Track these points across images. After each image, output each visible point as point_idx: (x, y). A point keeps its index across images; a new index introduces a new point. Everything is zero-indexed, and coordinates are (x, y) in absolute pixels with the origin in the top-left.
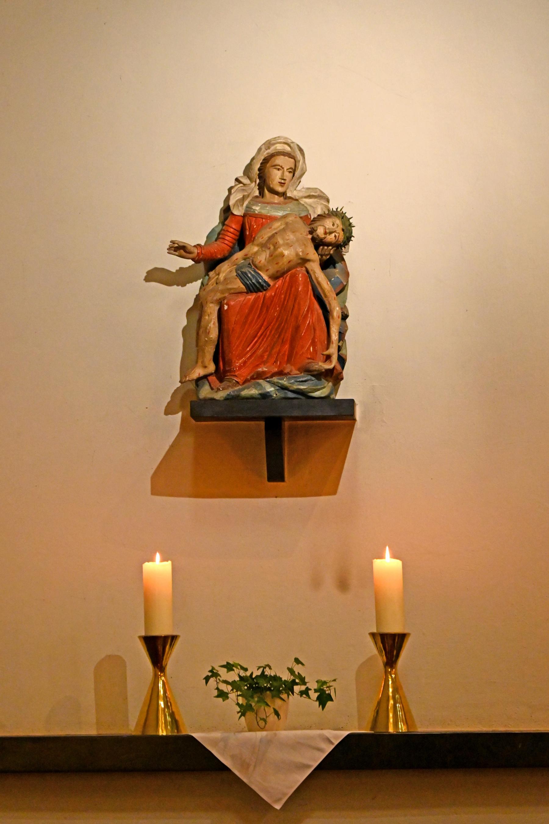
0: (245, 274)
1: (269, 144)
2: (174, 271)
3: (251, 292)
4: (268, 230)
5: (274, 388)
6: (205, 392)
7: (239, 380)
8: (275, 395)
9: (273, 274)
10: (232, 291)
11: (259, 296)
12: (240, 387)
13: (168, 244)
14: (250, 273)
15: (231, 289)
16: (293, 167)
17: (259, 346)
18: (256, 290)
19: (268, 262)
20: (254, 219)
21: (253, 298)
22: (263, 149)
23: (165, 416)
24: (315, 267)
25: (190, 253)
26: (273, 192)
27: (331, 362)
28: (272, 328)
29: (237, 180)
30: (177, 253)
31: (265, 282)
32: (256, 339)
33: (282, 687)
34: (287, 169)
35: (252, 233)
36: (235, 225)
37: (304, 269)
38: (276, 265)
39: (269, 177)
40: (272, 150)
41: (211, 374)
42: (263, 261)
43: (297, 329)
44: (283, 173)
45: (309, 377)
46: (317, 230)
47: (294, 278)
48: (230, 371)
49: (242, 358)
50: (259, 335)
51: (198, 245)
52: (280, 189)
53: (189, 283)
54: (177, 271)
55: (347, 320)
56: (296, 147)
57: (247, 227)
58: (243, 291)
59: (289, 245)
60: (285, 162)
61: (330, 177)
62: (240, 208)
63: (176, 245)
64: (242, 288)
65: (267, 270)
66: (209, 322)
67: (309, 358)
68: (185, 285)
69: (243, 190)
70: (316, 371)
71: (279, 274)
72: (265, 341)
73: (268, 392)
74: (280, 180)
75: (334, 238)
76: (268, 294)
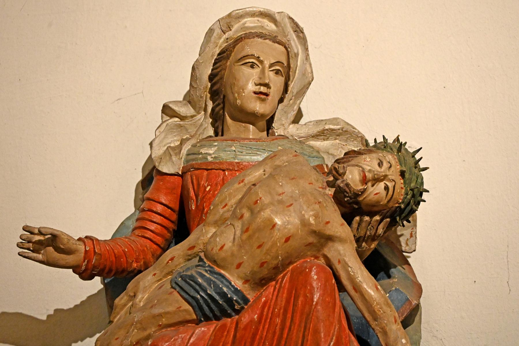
0: (189, 279)
1: (227, 22)
2: (44, 318)
3: (207, 319)
4: (236, 186)
9: (253, 273)
10: (164, 321)
11: (224, 326)
13: (17, 234)
14: (202, 276)
15: (160, 315)
18: (218, 313)
19: (240, 247)
20: (205, 173)
22: (218, 31)
24: (347, 256)
25: (68, 252)
26: (248, 117)
30: (40, 257)
31: (236, 291)
34: (271, 65)
36: (166, 194)
37: (322, 261)
38: (258, 251)
39: (232, 85)
40: (236, 31)
42: (229, 245)
44: (263, 71)
47: (300, 280)
51: (86, 237)
54: (49, 316)
56: (287, 20)
57: (192, 193)
58: (188, 317)
59: (285, 205)
61: (245, 215)
65: (239, 266)
69: (180, 126)
71: (265, 272)
74: (257, 89)
75: (384, 193)
76: (245, 318)
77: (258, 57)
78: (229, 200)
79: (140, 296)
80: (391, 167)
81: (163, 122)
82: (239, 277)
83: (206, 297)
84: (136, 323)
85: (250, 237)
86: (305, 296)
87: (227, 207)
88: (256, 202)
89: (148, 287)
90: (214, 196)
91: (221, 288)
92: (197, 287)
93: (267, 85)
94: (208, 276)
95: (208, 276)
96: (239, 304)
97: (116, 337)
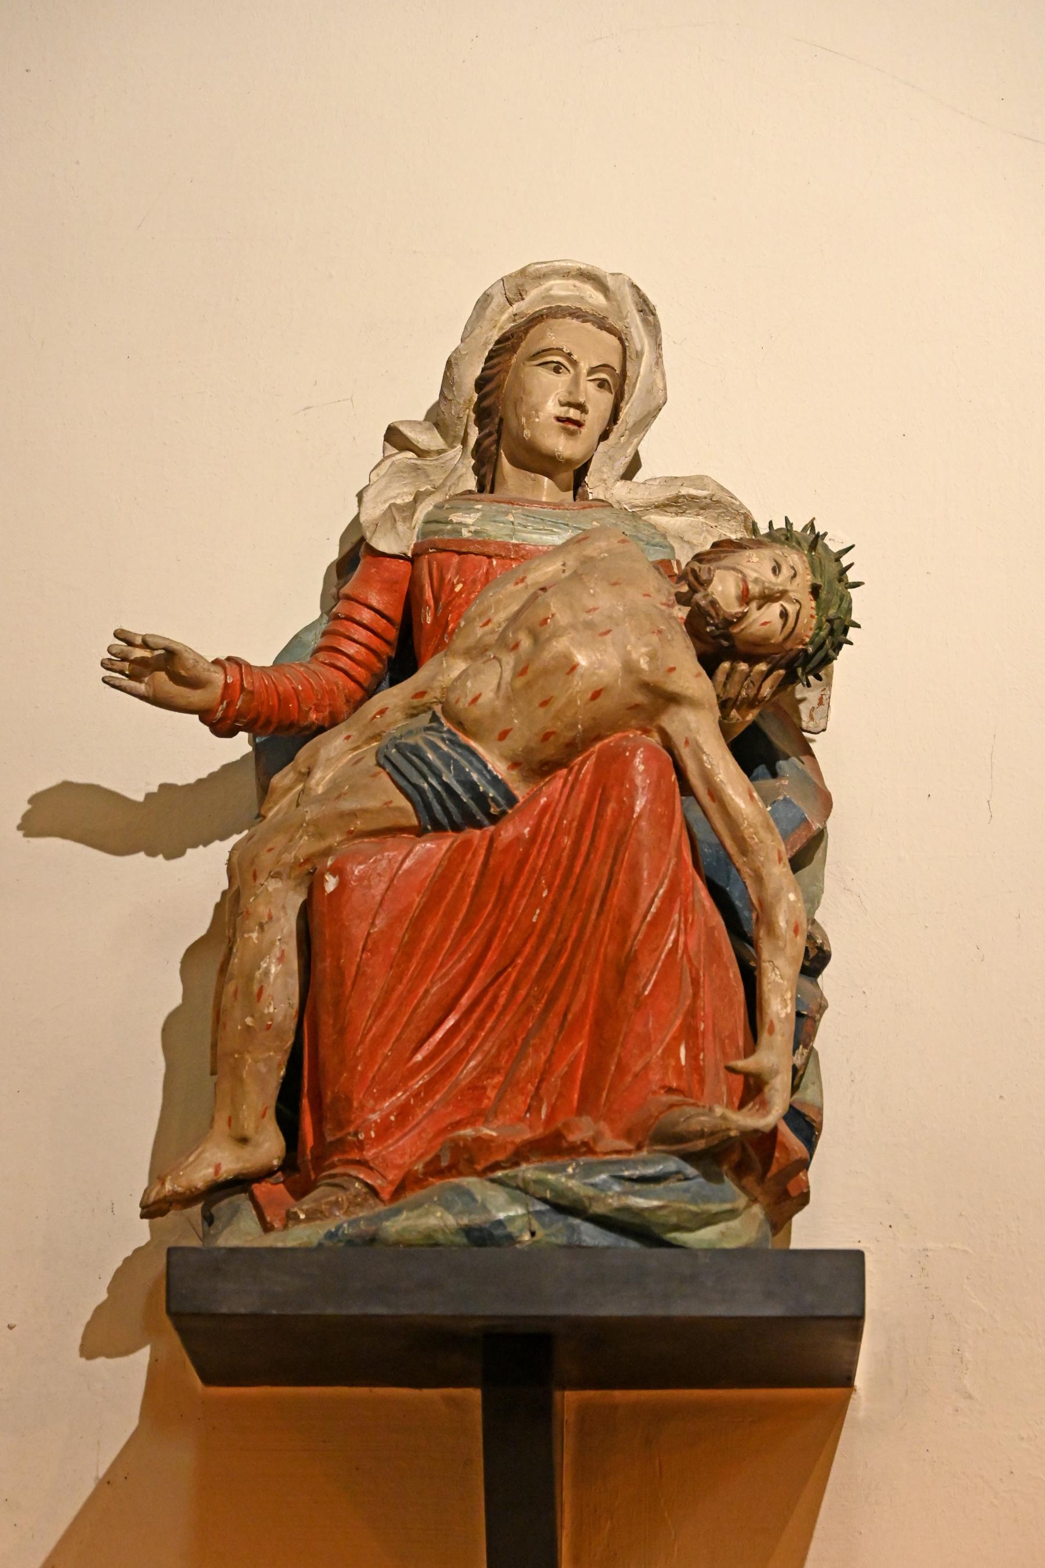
1: (517, 285)
2: (140, 798)
3: (438, 827)
4: (511, 587)
5: (526, 1206)
6: (242, 1231)
7: (377, 1182)
8: (527, 1237)
9: (528, 751)
10: (359, 824)
12: (381, 1208)
13: (104, 642)
14: (435, 748)
15: (353, 814)
16: (616, 363)
17: (465, 1049)
18: (457, 817)
19: (509, 700)
20: (456, 559)
21: (445, 847)
22: (499, 299)
23: (83, 1360)
25: (194, 683)
27: (765, 1106)
28: (522, 975)
29: (394, 437)
30: (142, 688)
32: (450, 1022)
33: (367, 1134)
34: (592, 371)
35: (445, 615)
36: (380, 592)
37: (655, 739)
38: (541, 711)
39: (517, 402)
40: (531, 304)
41: (265, 1174)
42: (488, 695)
43: (624, 969)
45: (672, 1164)
46: (709, 582)
47: (613, 771)
48: (341, 1144)
49: (393, 1092)
50: (465, 1001)
51: (229, 659)
52: (562, 446)
53: (195, 846)
54: (149, 796)
55: (827, 979)
56: (627, 290)
57: (428, 594)
58: (404, 822)
59: (596, 631)
60: (593, 348)
62: (401, 527)
63: (139, 653)
64: (401, 810)
65: (503, 735)
66: (261, 954)
67: (670, 1090)
68: (181, 853)
69: (416, 468)
70: (701, 1135)
71: (550, 751)
72: (493, 1029)
73: (500, 1223)
74: (562, 411)
75: (778, 622)
76: (507, 832)
77: (570, 354)
78: (496, 613)
79: (318, 775)
80: (795, 575)
81: (385, 458)
82: (503, 757)
83: (439, 788)
84: (308, 824)
85: (528, 685)
86: (620, 802)
87: (490, 626)
88: (544, 622)
89: (334, 756)
90: (468, 602)
91: (468, 774)
92: (425, 769)
93: (581, 407)
94: (446, 749)
95: (446, 749)
96: (498, 805)
97: (270, 846)
